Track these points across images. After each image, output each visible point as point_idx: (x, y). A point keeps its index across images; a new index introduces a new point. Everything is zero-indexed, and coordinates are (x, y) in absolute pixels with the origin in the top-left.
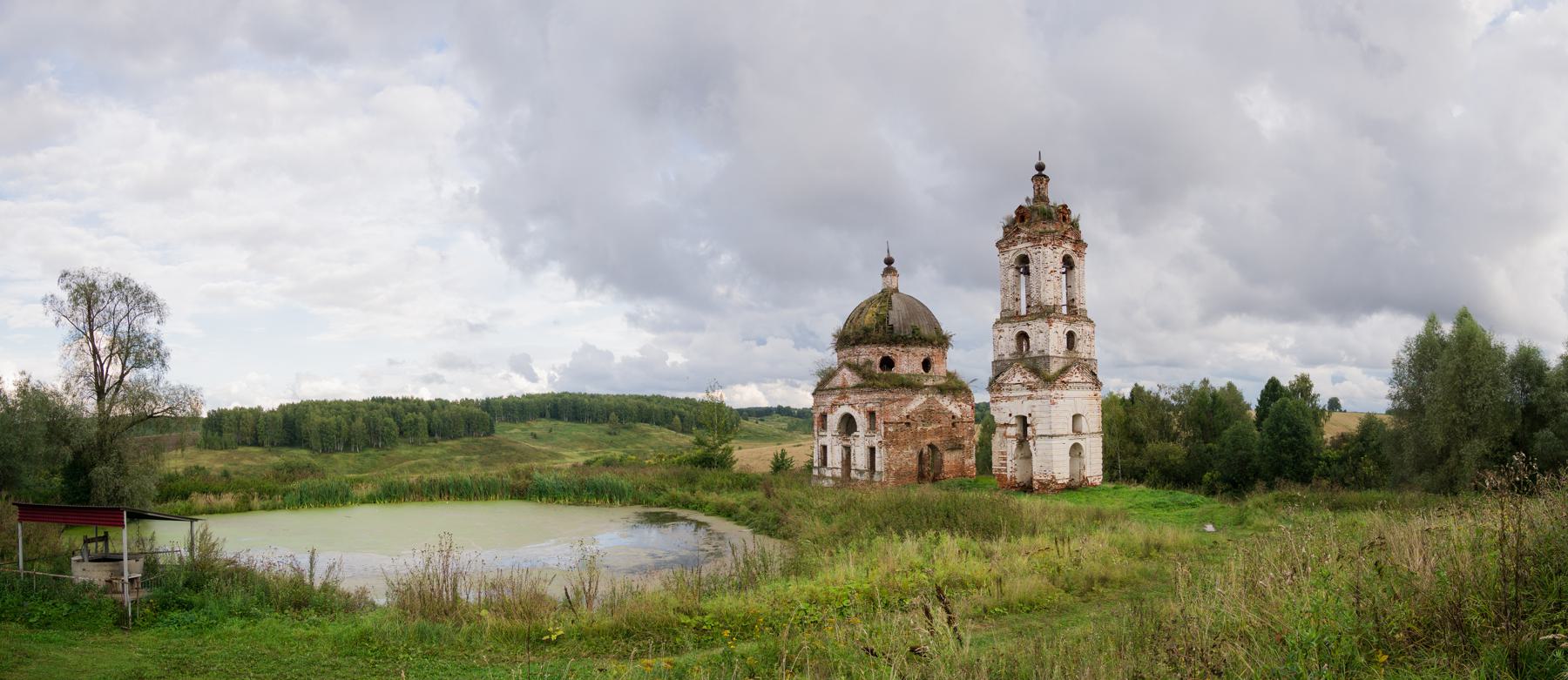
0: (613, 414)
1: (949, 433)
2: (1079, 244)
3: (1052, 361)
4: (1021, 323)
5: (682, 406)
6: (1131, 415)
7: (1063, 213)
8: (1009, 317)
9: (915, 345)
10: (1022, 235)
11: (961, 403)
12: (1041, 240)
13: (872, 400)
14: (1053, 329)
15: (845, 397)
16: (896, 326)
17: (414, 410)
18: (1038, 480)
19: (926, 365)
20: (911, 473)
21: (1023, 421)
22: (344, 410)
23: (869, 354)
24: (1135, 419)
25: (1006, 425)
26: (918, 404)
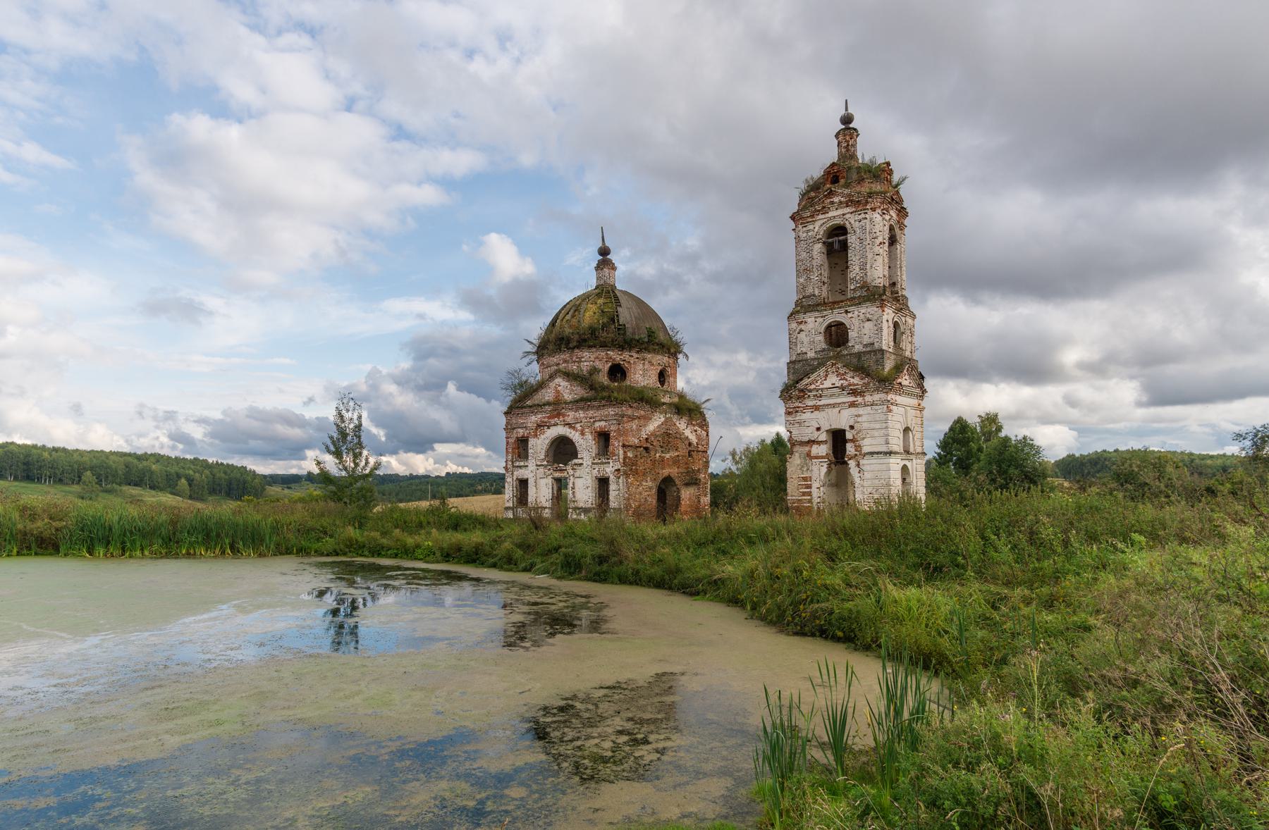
0: (89, 473)
1: (686, 464)
2: (902, 212)
4: (836, 311)
5: (189, 468)
10: (836, 200)
11: (696, 428)
12: (867, 202)
13: (604, 418)
15: (558, 415)
19: (662, 376)
20: (650, 511)
21: (838, 438)
23: (592, 360)
25: (811, 442)
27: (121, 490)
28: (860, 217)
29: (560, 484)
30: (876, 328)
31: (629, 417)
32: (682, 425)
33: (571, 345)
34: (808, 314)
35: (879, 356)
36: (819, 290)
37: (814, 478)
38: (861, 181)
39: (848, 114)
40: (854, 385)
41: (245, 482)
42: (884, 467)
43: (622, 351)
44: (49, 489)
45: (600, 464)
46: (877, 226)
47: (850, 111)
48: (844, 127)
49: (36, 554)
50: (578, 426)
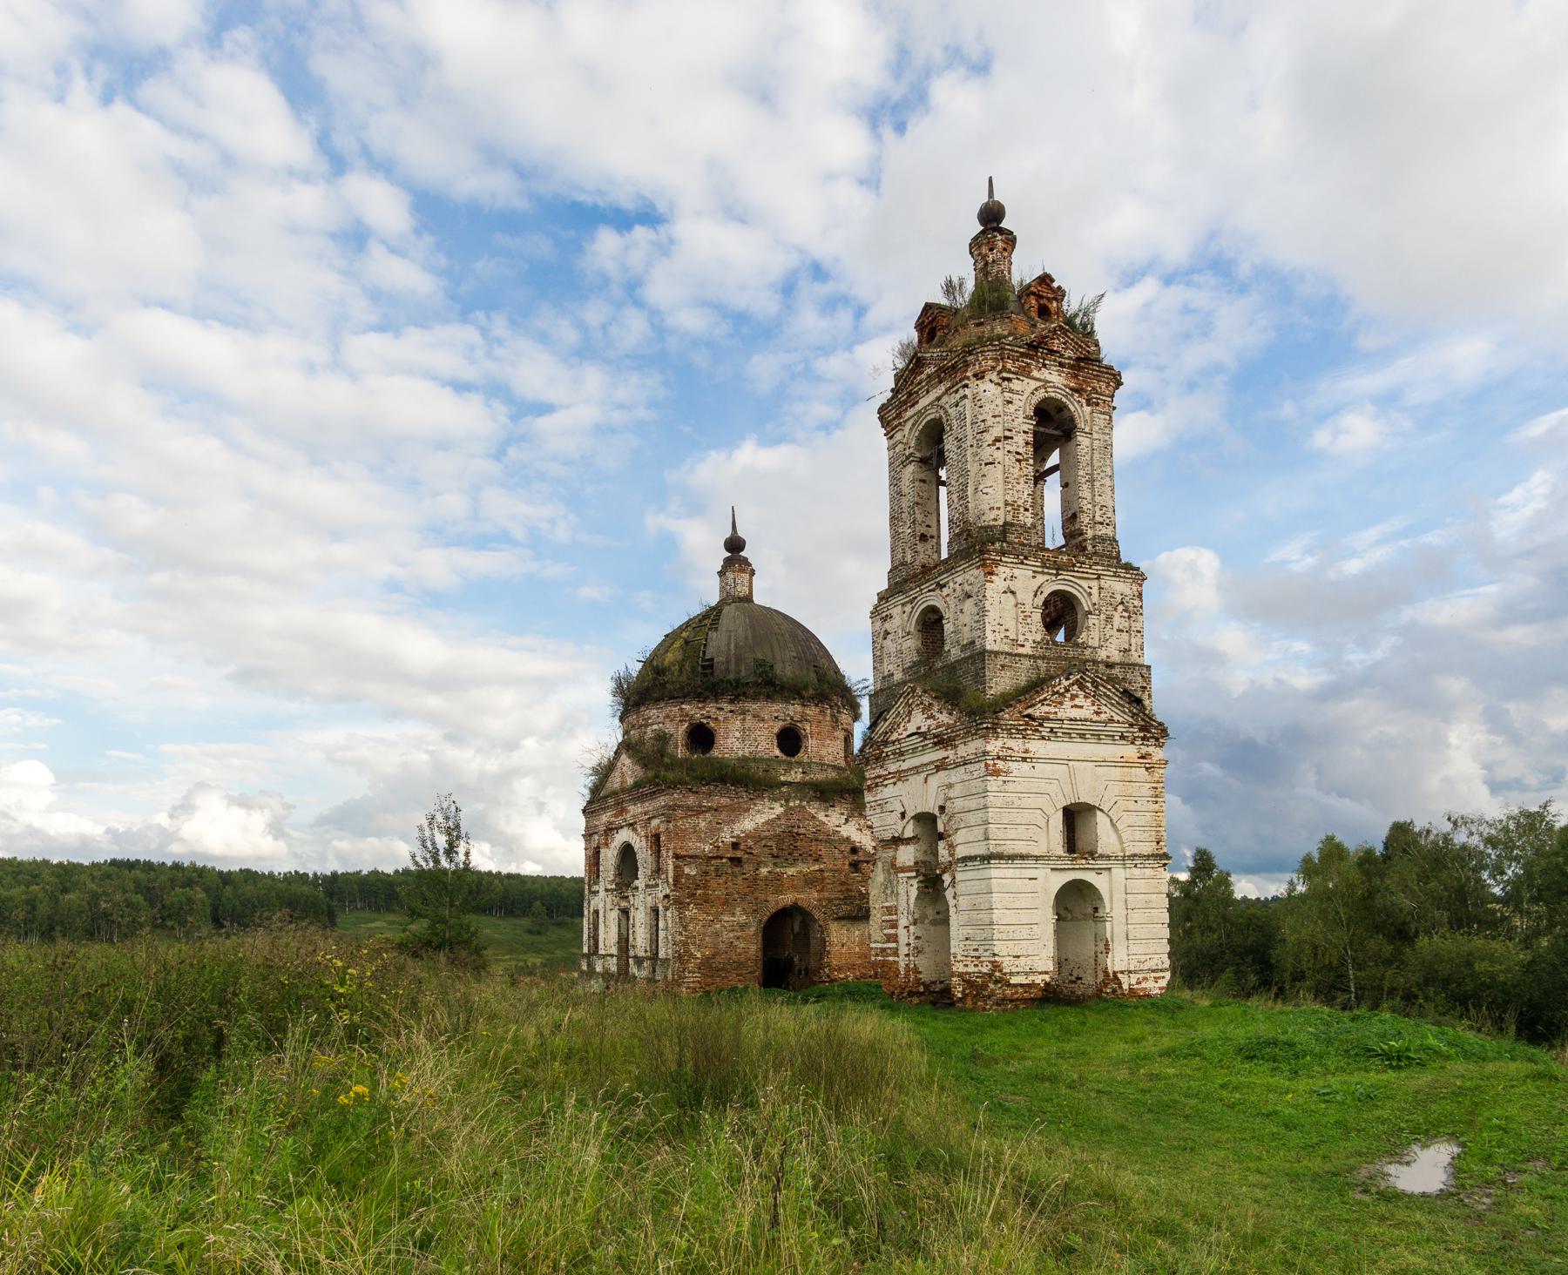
0: (538, 903)
3: (991, 667)
6: (1377, 881)
7: (1039, 297)
8: (903, 581)
9: (755, 698)
12: (967, 365)
14: (998, 584)
16: (719, 659)
17: (189, 883)
18: (961, 975)
22: (48, 878)
24: (1387, 888)
26: (761, 819)
27: (572, 923)
28: (958, 396)
31: (689, 808)
37: (901, 909)
39: (994, 201)
42: (983, 886)
43: (704, 702)
46: (986, 408)
47: (996, 198)
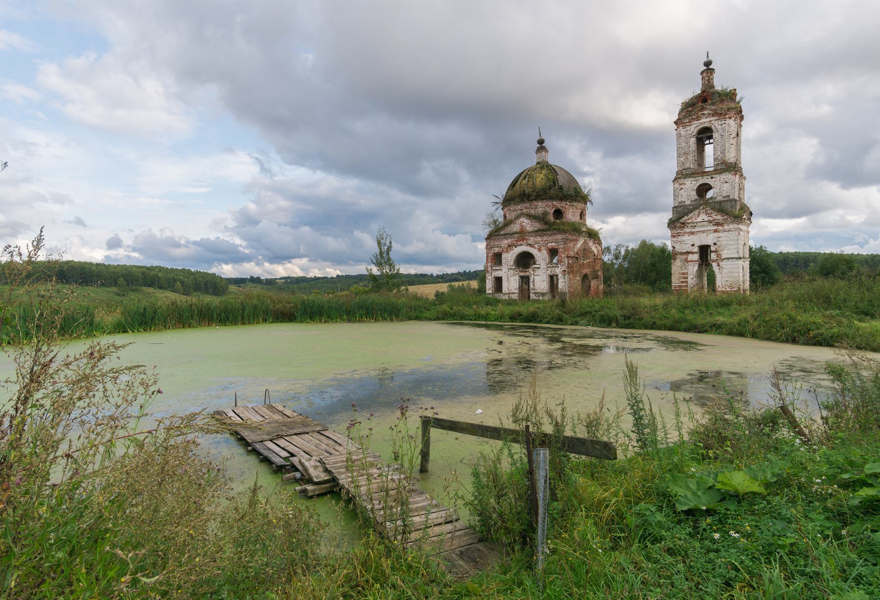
4: (705, 177)
5: (180, 275)
10: (706, 112)
11: (597, 245)
12: (726, 114)
15: (523, 240)
21: (704, 251)
23: (542, 207)
25: (688, 253)
28: (722, 122)
29: (525, 281)
30: (731, 187)
32: (591, 243)
33: (531, 198)
34: (687, 179)
35: (733, 203)
36: (691, 164)
37: (689, 273)
38: (722, 101)
40: (717, 220)
41: (216, 283)
44: (98, 290)
45: (553, 267)
46: (731, 128)
48: (706, 68)
49: (281, 322)
50: (536, 246)
